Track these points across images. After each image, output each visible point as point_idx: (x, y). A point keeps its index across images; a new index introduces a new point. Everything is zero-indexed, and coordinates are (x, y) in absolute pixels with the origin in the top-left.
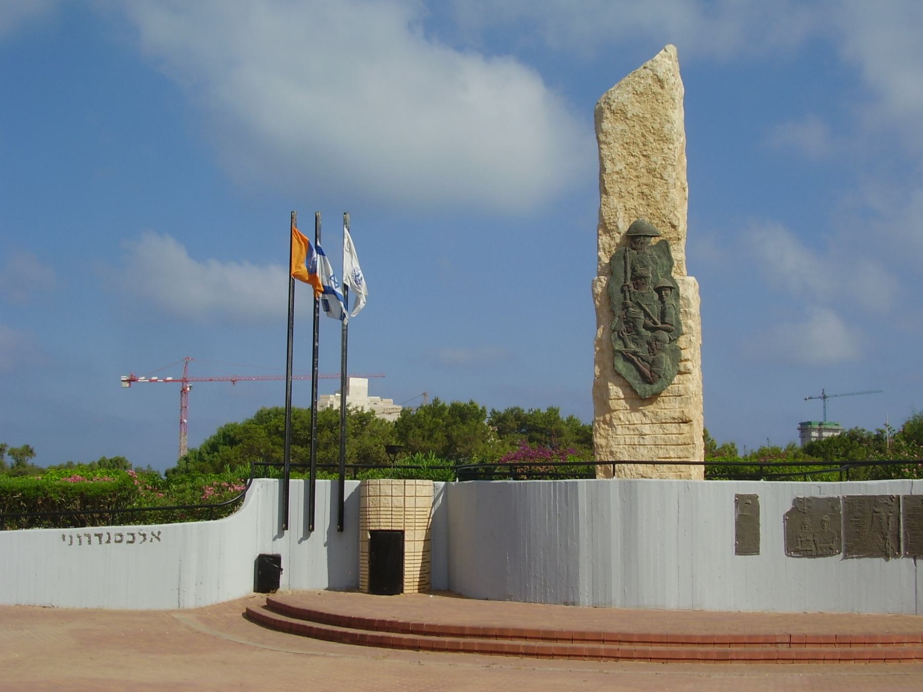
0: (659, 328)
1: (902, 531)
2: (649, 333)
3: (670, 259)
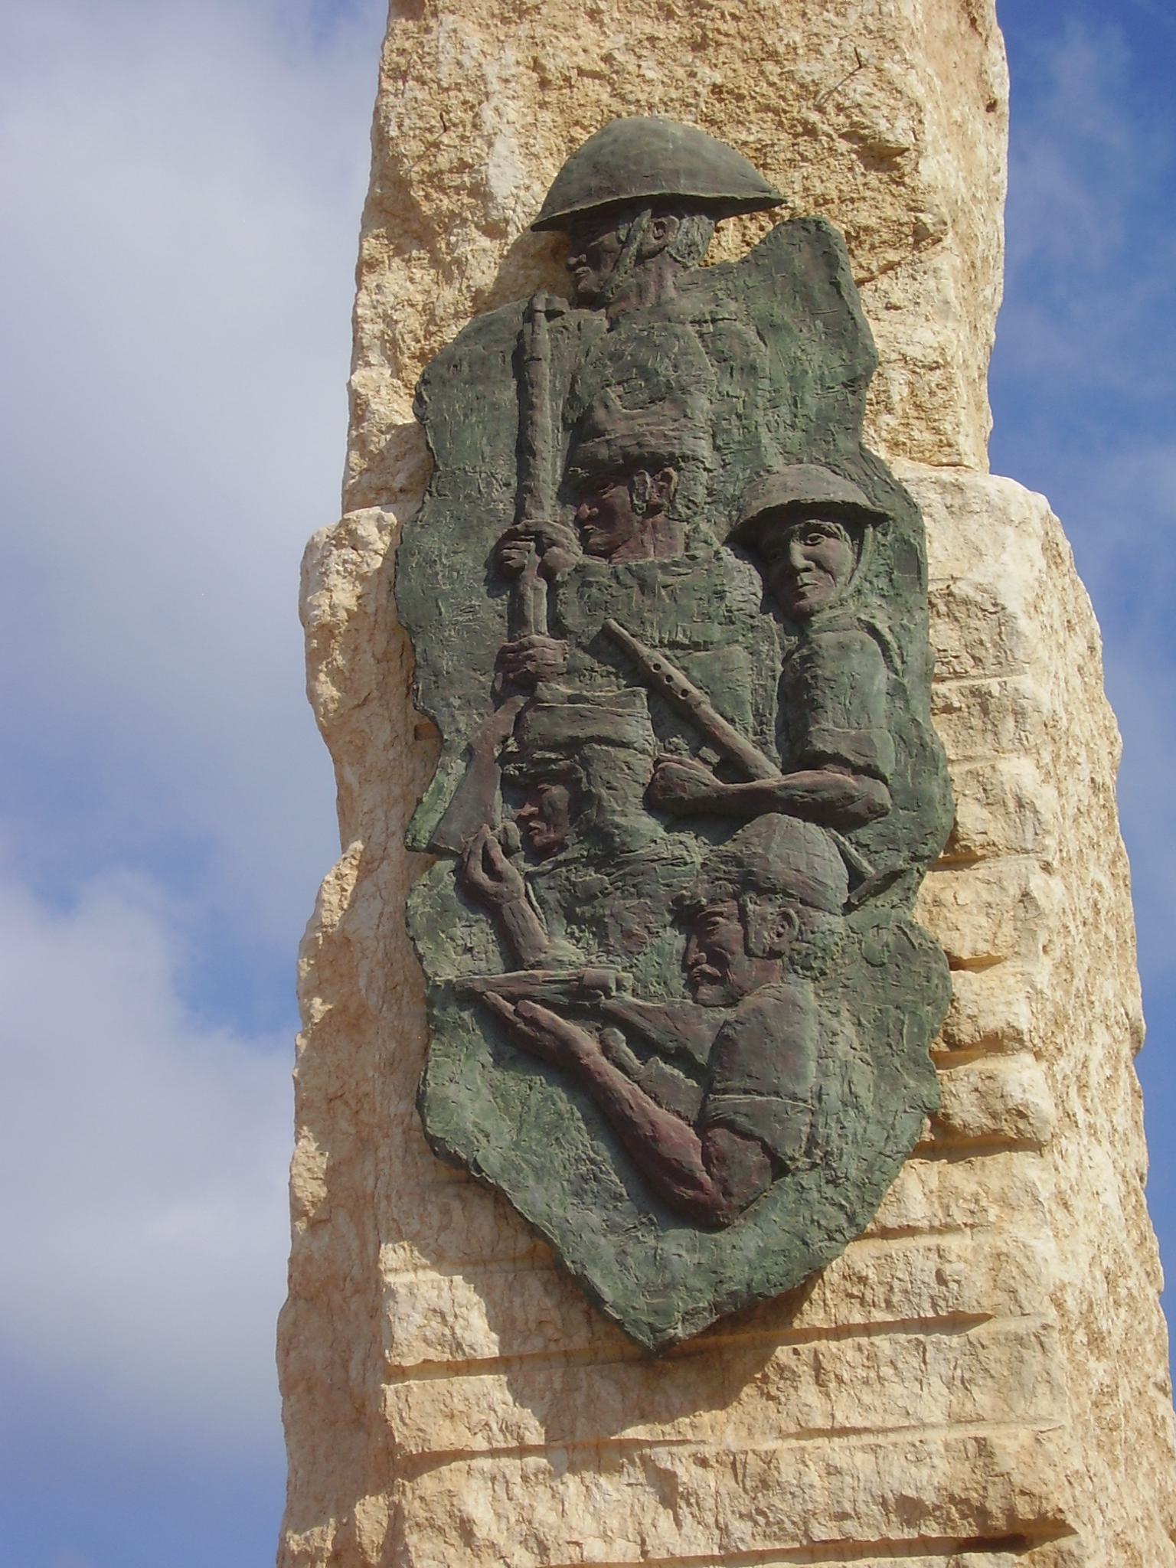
0: (765, 802)
2: (694, 848)
3: (846, 332)
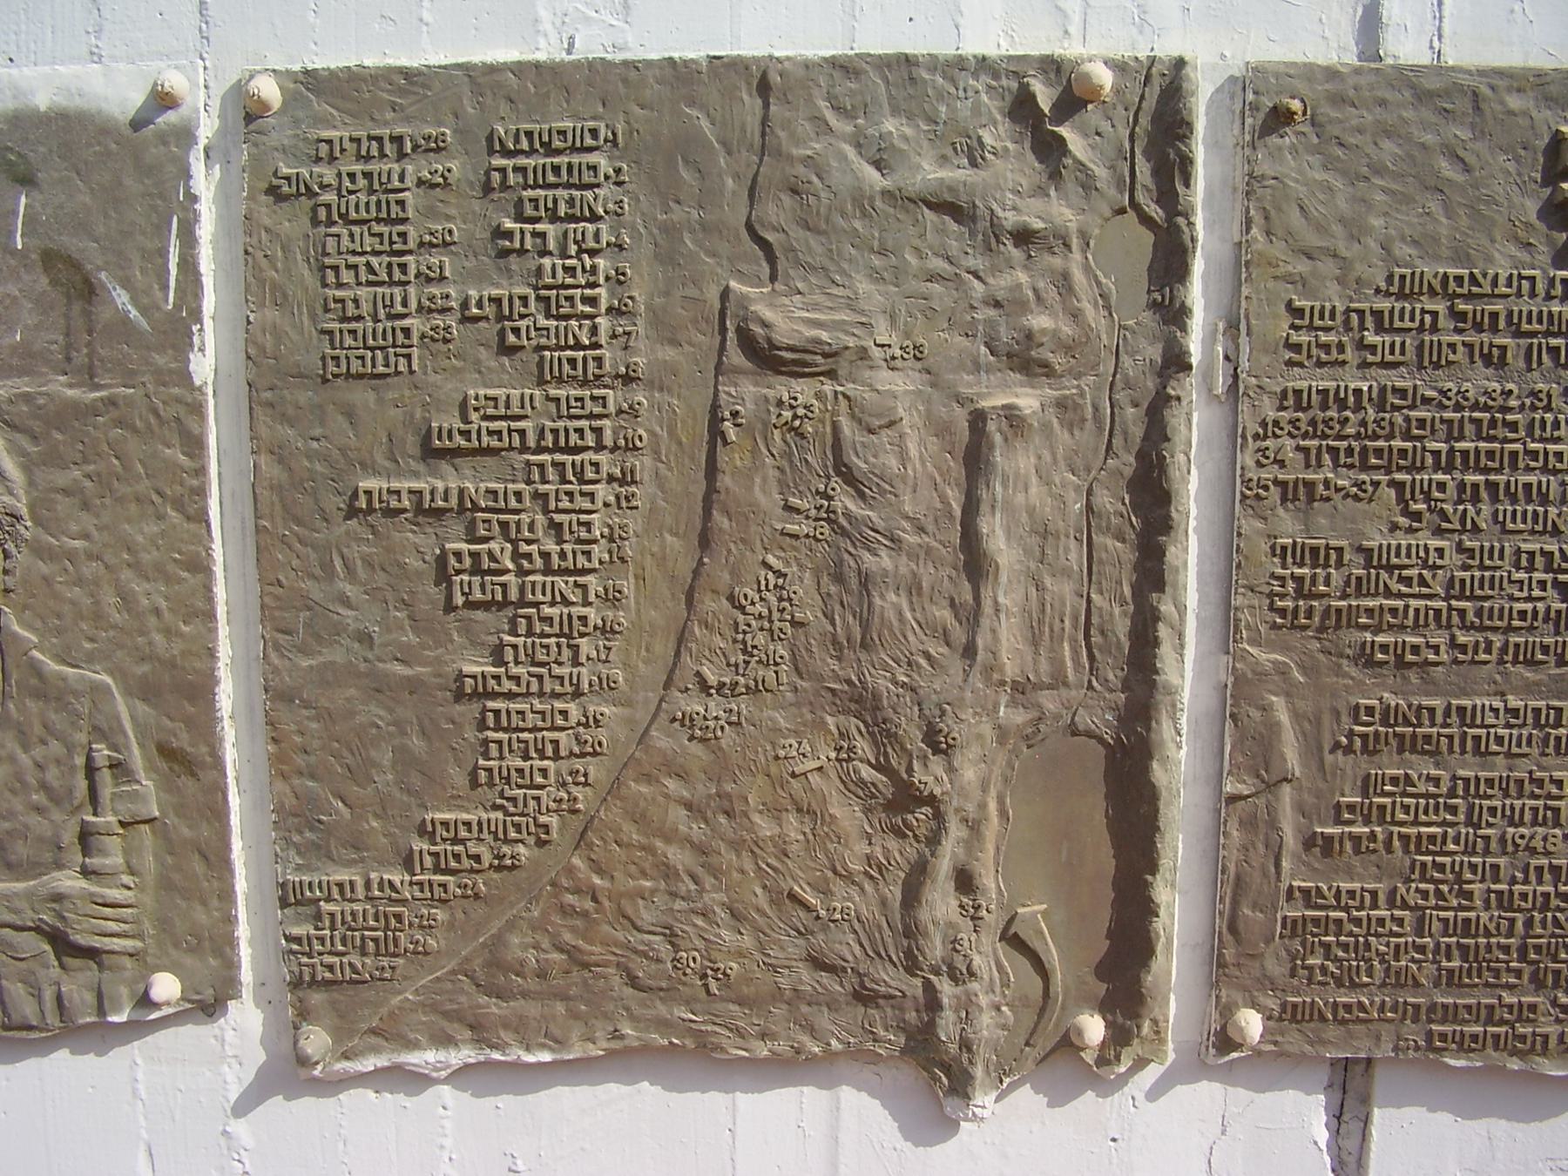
1: (1189, 671)
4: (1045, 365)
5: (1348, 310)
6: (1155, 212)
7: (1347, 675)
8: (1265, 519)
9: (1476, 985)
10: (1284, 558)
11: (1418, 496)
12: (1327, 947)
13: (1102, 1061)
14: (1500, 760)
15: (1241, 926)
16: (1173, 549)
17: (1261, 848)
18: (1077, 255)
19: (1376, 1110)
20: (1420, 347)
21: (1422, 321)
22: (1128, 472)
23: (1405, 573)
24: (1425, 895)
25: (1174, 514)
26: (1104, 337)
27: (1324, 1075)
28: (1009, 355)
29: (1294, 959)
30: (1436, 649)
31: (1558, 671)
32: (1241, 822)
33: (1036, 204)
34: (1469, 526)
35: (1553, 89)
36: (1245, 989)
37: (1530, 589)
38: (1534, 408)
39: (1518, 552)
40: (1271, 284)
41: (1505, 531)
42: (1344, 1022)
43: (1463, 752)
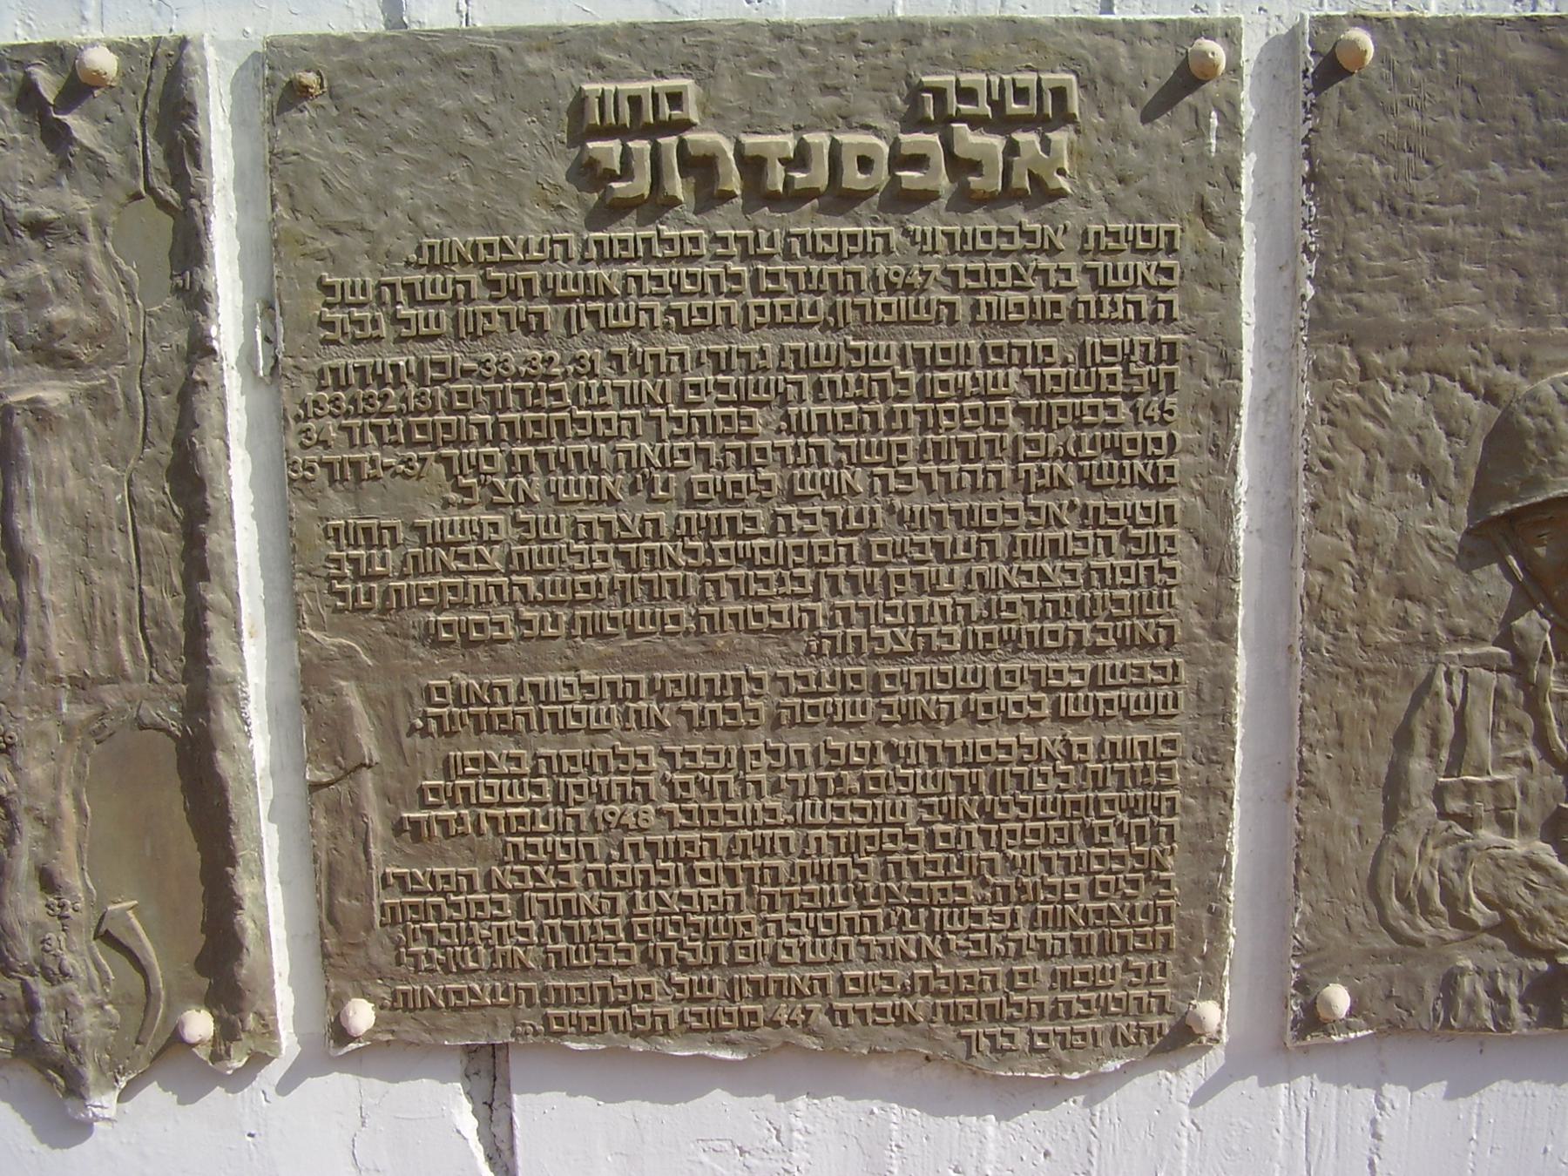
1: (254, 662)
4: (70, 356)
5: (380, 285)
6: (171, 194)
7: (414, 657)
8: (315, 501)
9: (587, 967)
10: (337, 540)
11: (467, 471)
12: (429, 932)
13: (215, 1057)
14: (581, 736)
15: (339, 916)
16: (214, 536)
17: (350, 837)
18: (94, 244)
19: (515, 1097)
20: (456, 319)
21: (455, 292)
22: (166, 460)
23: (462, 549)
24: (521, 876)
25: (210, 501)
26: (129, 325)
27: (457, 1063)
28: (34, 348)
29: (397, 947)
30: (501, 625)
31: (631, 643)
32: (327, 811)
33: (48, 193)
34: (522, 499)
35: (574, 47)
36: (353, 978)
37: (591, 561)
38: (577, 375)
39: (575, 523)
40: (301, 262)
41: (559, 502)
42: (456, 1009)
43: (542, 730)
